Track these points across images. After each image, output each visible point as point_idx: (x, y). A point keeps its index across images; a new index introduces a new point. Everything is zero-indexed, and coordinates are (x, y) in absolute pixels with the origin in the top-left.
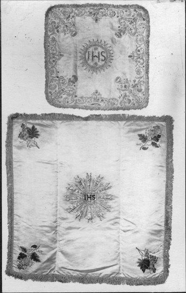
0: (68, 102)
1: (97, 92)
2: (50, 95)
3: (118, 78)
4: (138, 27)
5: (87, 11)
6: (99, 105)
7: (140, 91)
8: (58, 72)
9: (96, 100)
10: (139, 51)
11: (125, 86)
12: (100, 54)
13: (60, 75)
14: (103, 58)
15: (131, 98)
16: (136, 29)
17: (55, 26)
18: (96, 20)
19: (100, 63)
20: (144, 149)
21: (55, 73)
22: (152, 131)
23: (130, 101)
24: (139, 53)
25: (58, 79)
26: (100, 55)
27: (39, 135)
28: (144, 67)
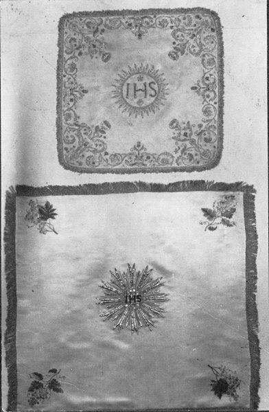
0: (94, 163)
1: (139, 146)
2: (65, 152)
3: (174, 121)
4: (203, 42)
5: (124, 21)
6: (144, 165)
7: (207, 140)
8: (79, 117)
9: (139, 159)
10: (207, 79)
11: (185, 135)
12: (147, 85)
13: (80, 121)
14: (153, 93)
15: (193, 153)
16: (201, 45)
17: (75, 45)
18: (140, 35)
19: (148, 101)
20: (212, 229)
21: (72, 119)
22: (223, 203)
23: (191, 157)
24: (207, 82)
25: (77, 128)
26: (148, 88)
27: (55, 214)
28: (215, 103)
